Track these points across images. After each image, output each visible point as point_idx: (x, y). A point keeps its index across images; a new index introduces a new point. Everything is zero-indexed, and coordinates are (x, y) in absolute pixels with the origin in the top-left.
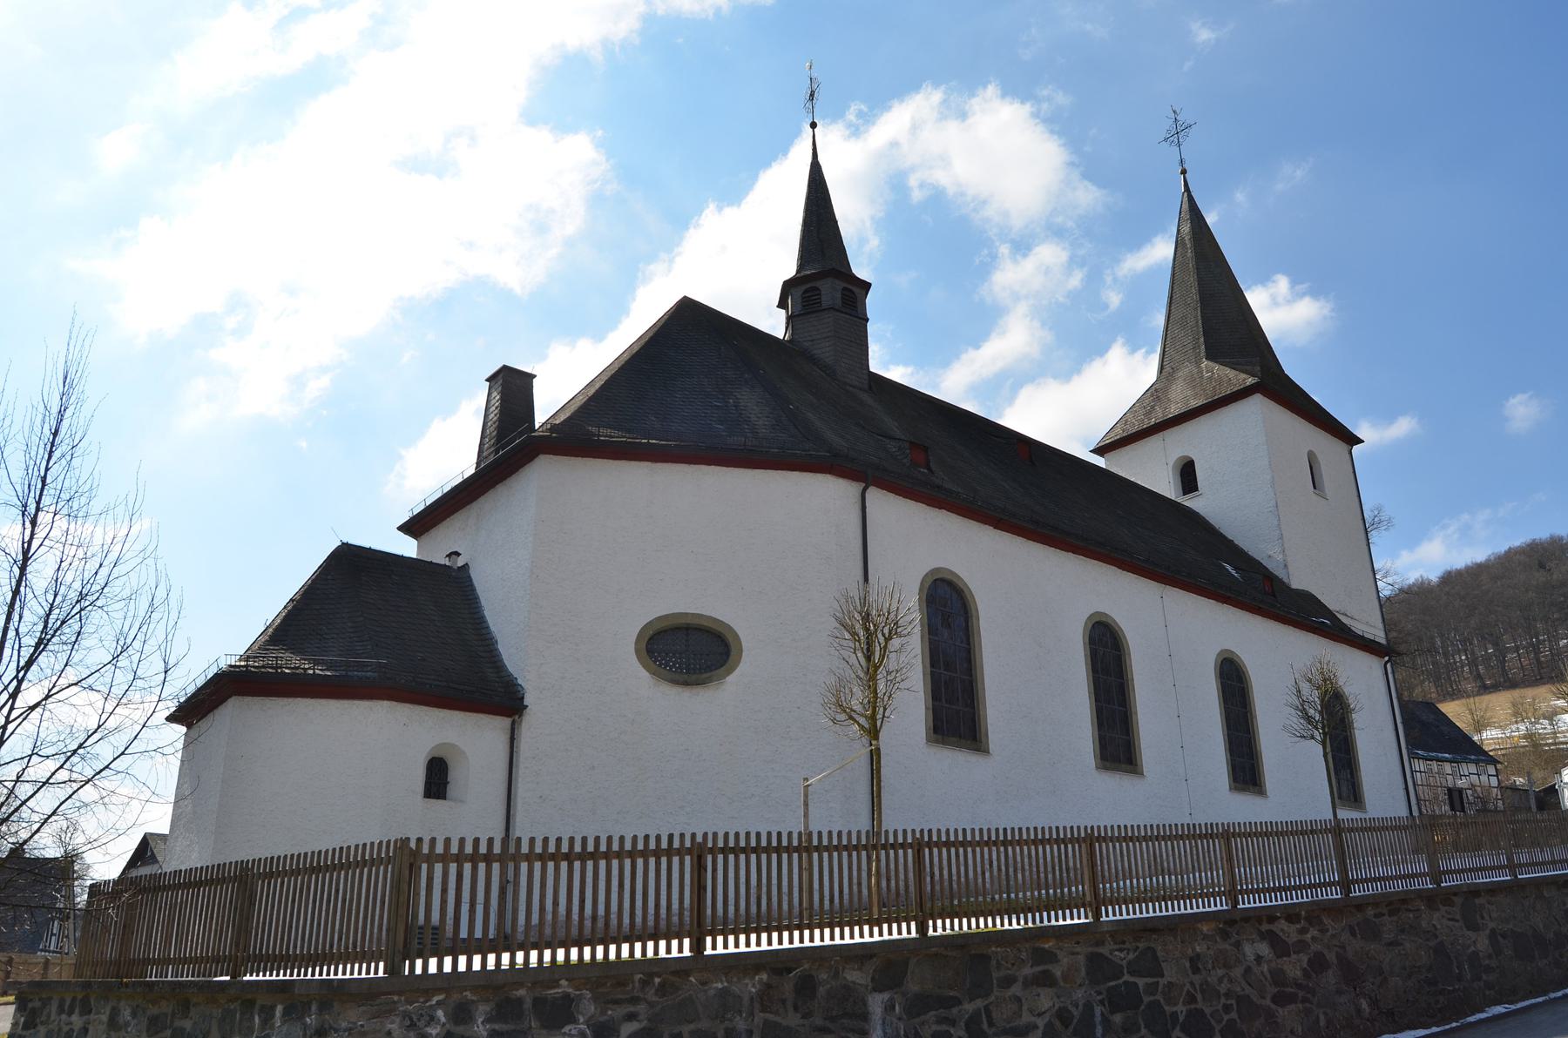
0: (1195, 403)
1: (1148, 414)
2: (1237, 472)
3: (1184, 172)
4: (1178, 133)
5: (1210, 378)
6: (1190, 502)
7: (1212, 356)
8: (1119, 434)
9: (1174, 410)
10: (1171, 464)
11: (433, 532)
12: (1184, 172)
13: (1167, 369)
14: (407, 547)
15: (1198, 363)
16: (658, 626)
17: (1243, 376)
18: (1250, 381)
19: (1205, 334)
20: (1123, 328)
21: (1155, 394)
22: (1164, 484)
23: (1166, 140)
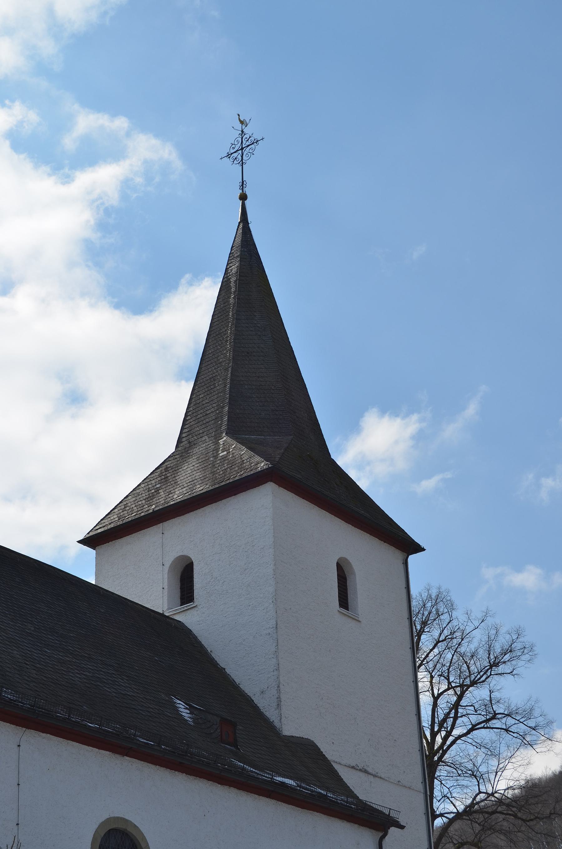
0: (200, 489)
1: (150, 498)
2: (245, 581)
3: (243, 197)
4: (241, 151)
5: (224, 458)
6: (189, 618)
7: (232, 432)
8: (115, 521)
9: (178, 495)
10: (167, 565)
11: (237, 496)
12: (243, 197)
13: (185, 443)
14: (83, 566)
15: (218, 437)
16: (130, 829)
17: (257, 458)
18: (263, 465)
19: (231, 404)
20: (187, 380)
21: (165, 472)
22: (153, 593)
23: (229, 155)
